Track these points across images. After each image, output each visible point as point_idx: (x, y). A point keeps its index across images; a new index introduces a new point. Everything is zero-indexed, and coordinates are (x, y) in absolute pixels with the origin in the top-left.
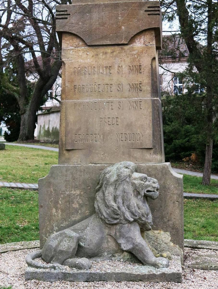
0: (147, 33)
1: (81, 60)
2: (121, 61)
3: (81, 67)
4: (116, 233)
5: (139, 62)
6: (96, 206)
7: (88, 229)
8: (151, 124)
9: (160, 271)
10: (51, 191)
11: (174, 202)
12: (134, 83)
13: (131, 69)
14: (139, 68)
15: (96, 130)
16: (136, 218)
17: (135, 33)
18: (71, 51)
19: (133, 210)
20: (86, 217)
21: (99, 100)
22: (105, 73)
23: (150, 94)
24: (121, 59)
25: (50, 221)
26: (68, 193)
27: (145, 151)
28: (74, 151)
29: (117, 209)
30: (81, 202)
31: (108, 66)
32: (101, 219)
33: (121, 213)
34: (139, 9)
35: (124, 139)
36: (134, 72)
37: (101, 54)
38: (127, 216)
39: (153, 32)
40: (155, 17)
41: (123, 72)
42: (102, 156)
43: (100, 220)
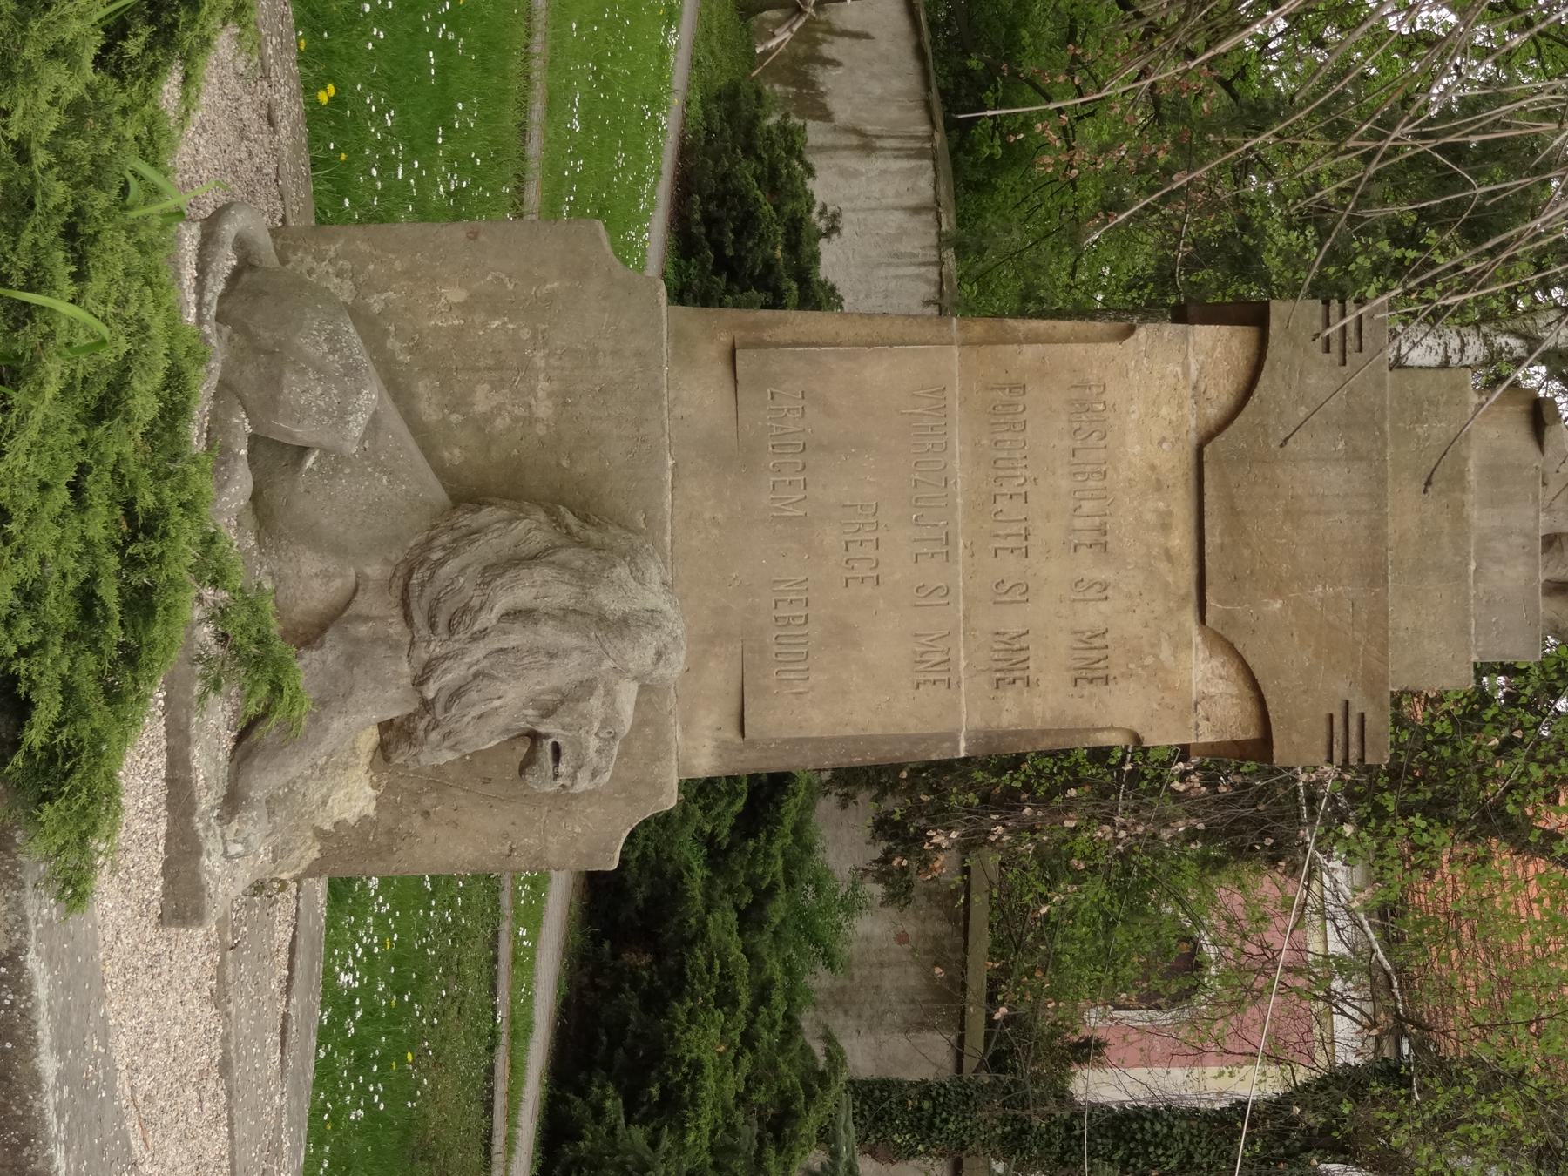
0: (1251, 708)
1: (1136, 411)
2: (1129, 596)
3: (1106, 414)
4: (367, 619)
5: (1123, 675)
6: (486, 515)
7: (380, 480)
8: (850, 731)
9: (208, 827)
10: (545, 282)
11: (506, 836)
12: (1031, 653)
13: (1091, 639)
14: (1096, 674)
15: (824, 486)
16: (439, 707)
17: (1250, 661)
18: (1179, 370)
19: (474, 695)
20: (428, 449)
21: (959, 500)
22: (1078, 523)
23: (983, 724)
24: (1138, 596)
25: (408, 274)
26: (537, 360)
27: (734, 706)
28: (729, 384)
29: (476, 628)
30: (500, 423)
31: (1108, 538)
32: (427, 545)
33: (457, 646)
34: (1354, 675)
35: (784, 611)
36: (1078, 654)
37: (1161, 504)
38: (444, 672)
39: (1253, 734)
40: (1321, 745)
41: (1079, 606)
42: (707, 515)
43: (422, 538)
